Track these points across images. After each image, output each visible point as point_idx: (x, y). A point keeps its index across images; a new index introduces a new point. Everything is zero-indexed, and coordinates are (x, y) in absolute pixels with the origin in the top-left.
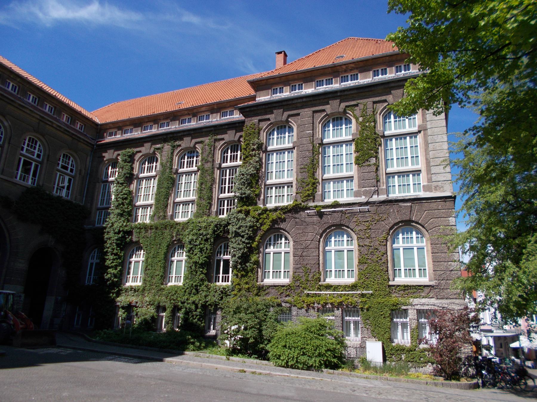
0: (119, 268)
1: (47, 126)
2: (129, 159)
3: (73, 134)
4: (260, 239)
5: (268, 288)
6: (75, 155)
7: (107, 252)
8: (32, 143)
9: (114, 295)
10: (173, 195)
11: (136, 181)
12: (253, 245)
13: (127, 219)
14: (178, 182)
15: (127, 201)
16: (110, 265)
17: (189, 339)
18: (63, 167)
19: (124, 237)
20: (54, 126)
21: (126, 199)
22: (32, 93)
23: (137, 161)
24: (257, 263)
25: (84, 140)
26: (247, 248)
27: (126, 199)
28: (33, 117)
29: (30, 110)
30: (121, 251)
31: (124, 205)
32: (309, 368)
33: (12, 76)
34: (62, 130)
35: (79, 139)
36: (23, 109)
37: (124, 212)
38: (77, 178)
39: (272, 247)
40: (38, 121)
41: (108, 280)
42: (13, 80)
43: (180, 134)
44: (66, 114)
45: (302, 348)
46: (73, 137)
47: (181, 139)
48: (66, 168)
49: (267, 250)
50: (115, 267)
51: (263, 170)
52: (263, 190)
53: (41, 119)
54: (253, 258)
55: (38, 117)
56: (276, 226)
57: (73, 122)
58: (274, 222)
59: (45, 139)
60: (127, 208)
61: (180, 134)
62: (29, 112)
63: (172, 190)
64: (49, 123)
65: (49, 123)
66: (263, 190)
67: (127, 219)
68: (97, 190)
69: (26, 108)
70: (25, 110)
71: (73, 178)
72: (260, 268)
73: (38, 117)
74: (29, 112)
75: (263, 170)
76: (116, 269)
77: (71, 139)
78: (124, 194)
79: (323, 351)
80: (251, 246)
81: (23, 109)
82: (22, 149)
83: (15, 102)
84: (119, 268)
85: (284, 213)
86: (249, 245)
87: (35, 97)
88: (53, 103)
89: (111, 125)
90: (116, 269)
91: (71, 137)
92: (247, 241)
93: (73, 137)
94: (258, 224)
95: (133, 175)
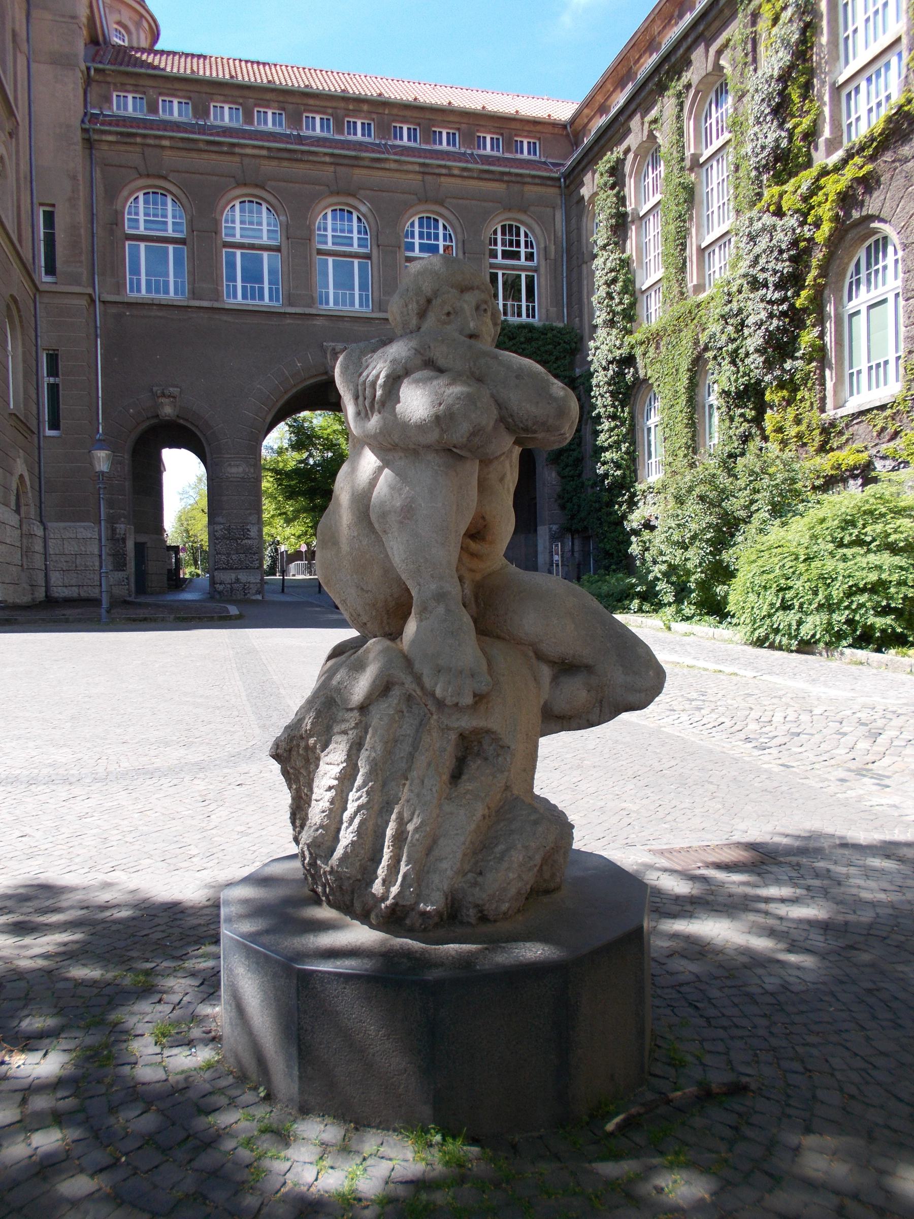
0: (624, 447)
1: (443, 179)
2: (611, 180)
3: (503, 173)
4: (820, 276)
5: (847, 426)
6: (523, 217)
7: (599, 416)
8: (429, 227)
9: (624, 507)
10: (694, 230)
11: (633, 227)
12: (799, 303)
13: (625, 328)
14: (705, 191)
15: (619, 286)
16: (606, 444)
17: (634, 586)
18: (506, 255)
19: (620, 374)
20: (456, 172)
21: (614, 281)
22: (402, 122)
23: (630, 177)
24: (819, 354)
25: (534, 177)
26: (784, 314)
27: (614, 281)
28: (407, 172)
29: (396, 161)
30: (622, 407)
31: (612, 298)
32: (806, 647)
33: (351, 107)
34: (475, 175)
35: (519, 179)
36: (383, 165)
37: (615, 313)
38: (542, 270)
39: (863, 288)
40: (419, 177)
41: (606, 475)
42: (356, 112)
43: (681, 51)
44: (490, 132)
45: (781, 589)
46: (506, 178)
47: (687, 63)
48: (516, 255)
49: (851, 307)
50: (617, 445)
51: (824, 40)
52: (827, 110)
53: (422, 170)
54: (807, 338)
55: (417, 168)
56: (856, 214)
57: (512, 145)
58: (846, 200)
59: (447, 208)
60: (621, 303)
61: (681, 51)
62: (393, 166)
63: (691, 219)
64: (444, 171)
65: (444, 171)
66: (827, 110)
67: (625, 328)
68: (585, 282)
69: (386, 160)
70: (387, 166)
71: (535, 271)
72: (831, 368)
73: (417, 168)
74: (393, 166)
75: (824, 40)
76: (619, 449)
77: (504, 186)
78: (612, 270)
79: (837, 593)
80: (792, 306)
81: (383, 165)
82: (411, 247)
83: (362, 159)
84: (624, 447)
85: (872, 158)
86: (785, 307)
87: (412, 127)
88: (450, 122)
89: (586, 111)
90: (619, 449)
91: (502, 181)
92: (777, 295)
93: (506, 178)
94: (806, 228)
95: (625, 215)
